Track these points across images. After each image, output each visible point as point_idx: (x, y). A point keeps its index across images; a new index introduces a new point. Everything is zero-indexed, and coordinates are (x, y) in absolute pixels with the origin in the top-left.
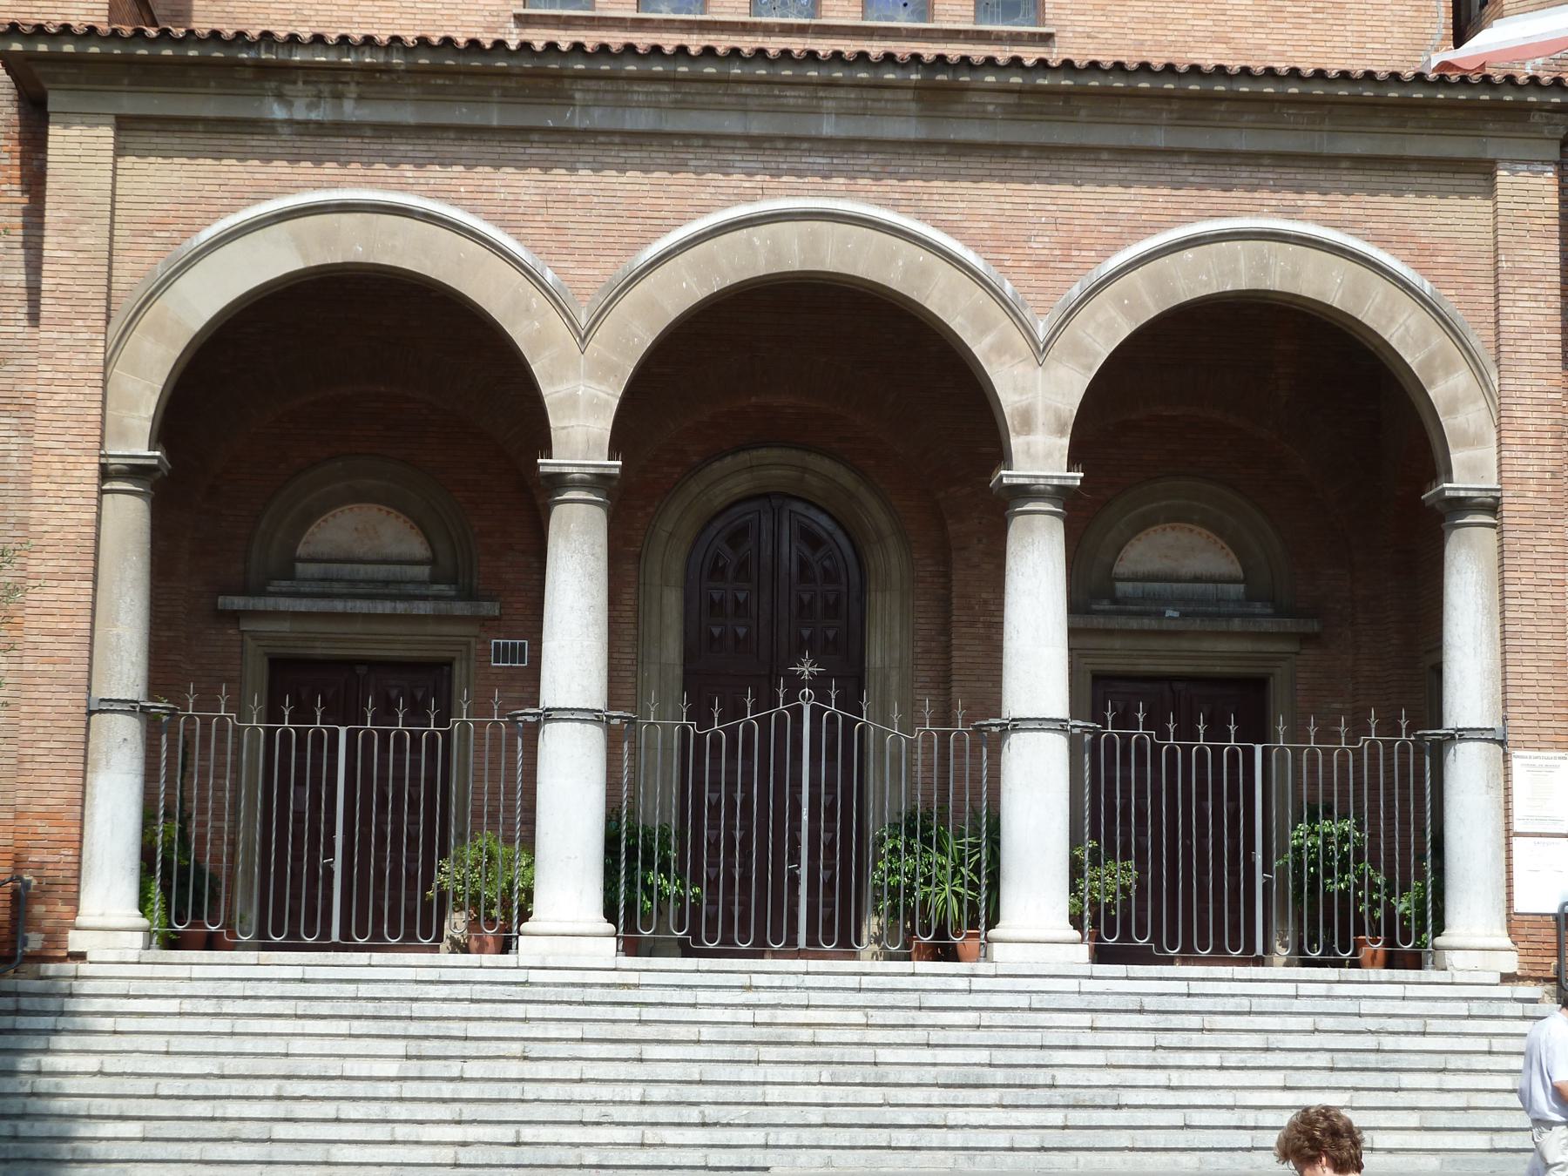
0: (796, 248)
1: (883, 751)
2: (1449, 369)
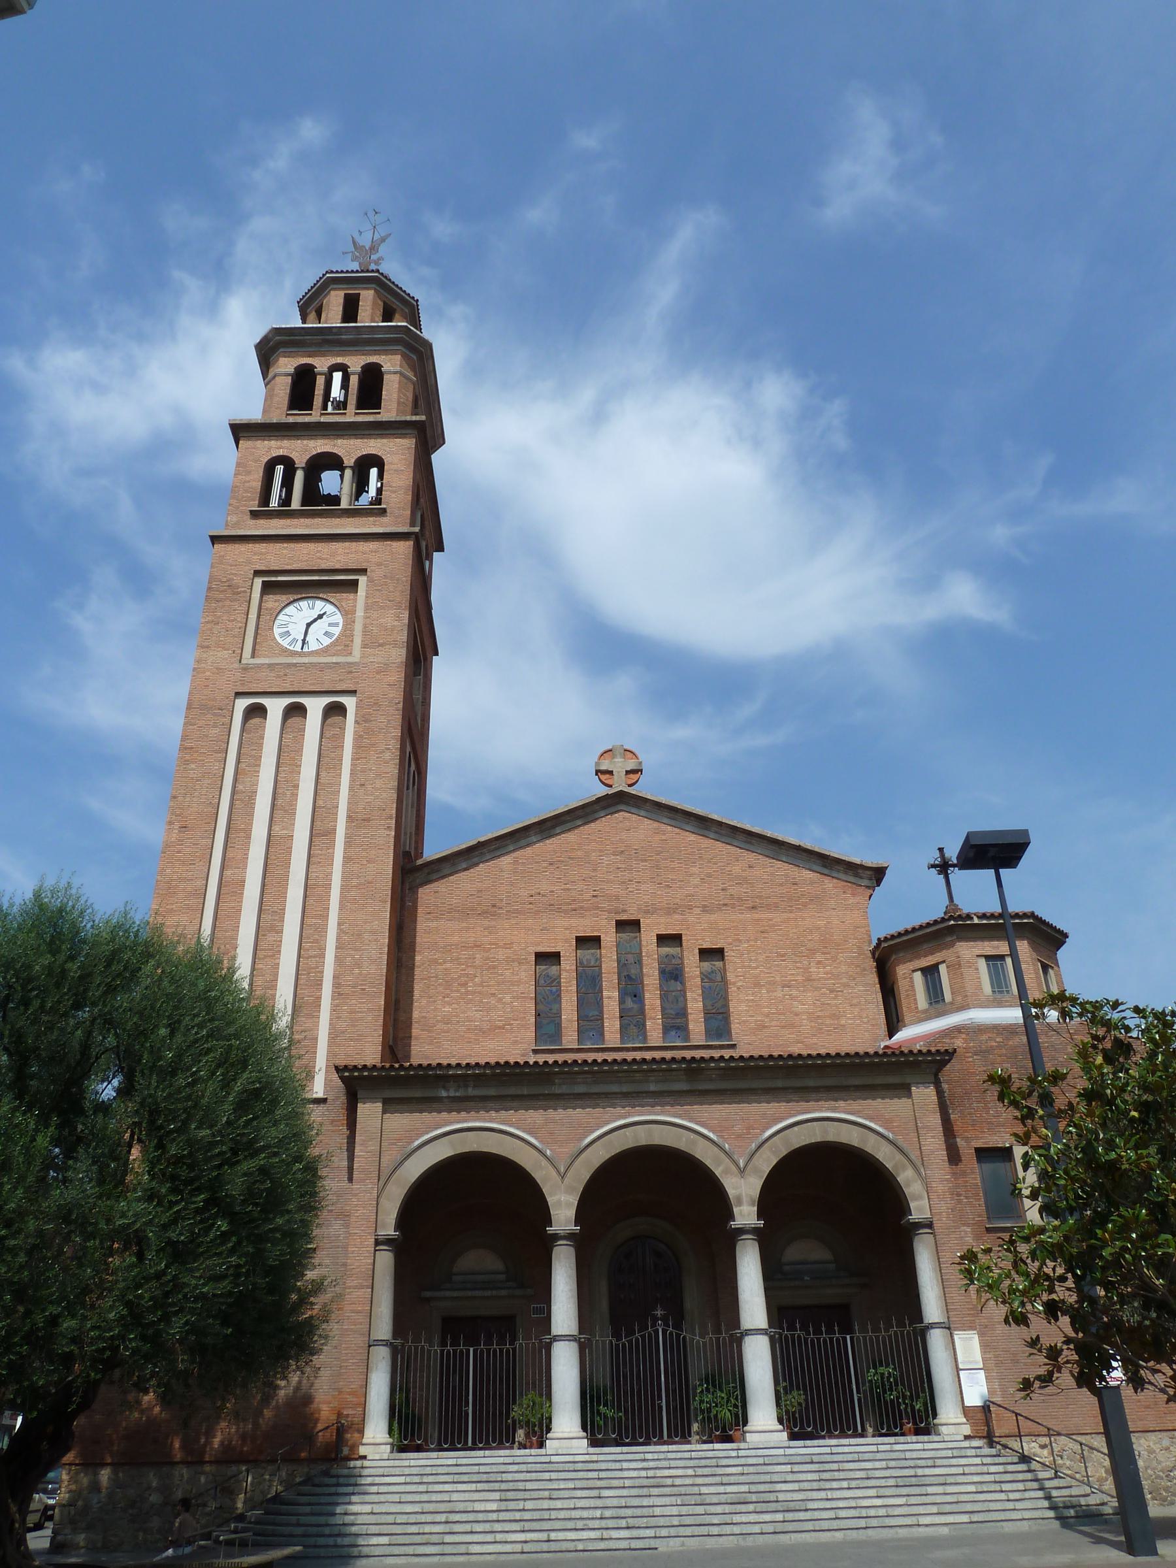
2: (904, 1168)
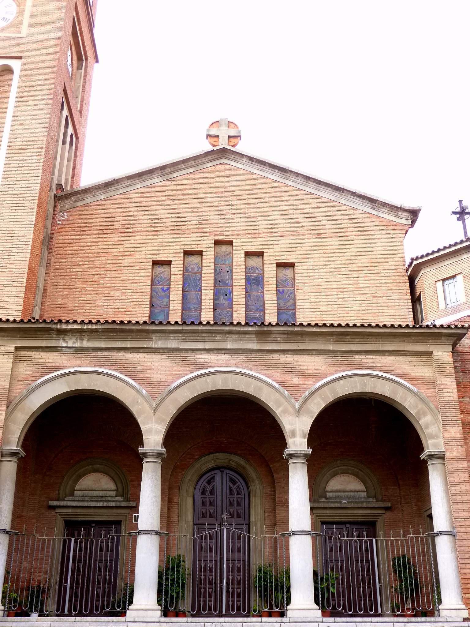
0: (220, 382)
1: (256, 548)
2: (425, 414)
